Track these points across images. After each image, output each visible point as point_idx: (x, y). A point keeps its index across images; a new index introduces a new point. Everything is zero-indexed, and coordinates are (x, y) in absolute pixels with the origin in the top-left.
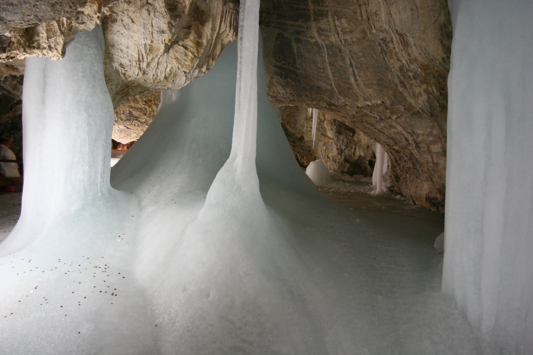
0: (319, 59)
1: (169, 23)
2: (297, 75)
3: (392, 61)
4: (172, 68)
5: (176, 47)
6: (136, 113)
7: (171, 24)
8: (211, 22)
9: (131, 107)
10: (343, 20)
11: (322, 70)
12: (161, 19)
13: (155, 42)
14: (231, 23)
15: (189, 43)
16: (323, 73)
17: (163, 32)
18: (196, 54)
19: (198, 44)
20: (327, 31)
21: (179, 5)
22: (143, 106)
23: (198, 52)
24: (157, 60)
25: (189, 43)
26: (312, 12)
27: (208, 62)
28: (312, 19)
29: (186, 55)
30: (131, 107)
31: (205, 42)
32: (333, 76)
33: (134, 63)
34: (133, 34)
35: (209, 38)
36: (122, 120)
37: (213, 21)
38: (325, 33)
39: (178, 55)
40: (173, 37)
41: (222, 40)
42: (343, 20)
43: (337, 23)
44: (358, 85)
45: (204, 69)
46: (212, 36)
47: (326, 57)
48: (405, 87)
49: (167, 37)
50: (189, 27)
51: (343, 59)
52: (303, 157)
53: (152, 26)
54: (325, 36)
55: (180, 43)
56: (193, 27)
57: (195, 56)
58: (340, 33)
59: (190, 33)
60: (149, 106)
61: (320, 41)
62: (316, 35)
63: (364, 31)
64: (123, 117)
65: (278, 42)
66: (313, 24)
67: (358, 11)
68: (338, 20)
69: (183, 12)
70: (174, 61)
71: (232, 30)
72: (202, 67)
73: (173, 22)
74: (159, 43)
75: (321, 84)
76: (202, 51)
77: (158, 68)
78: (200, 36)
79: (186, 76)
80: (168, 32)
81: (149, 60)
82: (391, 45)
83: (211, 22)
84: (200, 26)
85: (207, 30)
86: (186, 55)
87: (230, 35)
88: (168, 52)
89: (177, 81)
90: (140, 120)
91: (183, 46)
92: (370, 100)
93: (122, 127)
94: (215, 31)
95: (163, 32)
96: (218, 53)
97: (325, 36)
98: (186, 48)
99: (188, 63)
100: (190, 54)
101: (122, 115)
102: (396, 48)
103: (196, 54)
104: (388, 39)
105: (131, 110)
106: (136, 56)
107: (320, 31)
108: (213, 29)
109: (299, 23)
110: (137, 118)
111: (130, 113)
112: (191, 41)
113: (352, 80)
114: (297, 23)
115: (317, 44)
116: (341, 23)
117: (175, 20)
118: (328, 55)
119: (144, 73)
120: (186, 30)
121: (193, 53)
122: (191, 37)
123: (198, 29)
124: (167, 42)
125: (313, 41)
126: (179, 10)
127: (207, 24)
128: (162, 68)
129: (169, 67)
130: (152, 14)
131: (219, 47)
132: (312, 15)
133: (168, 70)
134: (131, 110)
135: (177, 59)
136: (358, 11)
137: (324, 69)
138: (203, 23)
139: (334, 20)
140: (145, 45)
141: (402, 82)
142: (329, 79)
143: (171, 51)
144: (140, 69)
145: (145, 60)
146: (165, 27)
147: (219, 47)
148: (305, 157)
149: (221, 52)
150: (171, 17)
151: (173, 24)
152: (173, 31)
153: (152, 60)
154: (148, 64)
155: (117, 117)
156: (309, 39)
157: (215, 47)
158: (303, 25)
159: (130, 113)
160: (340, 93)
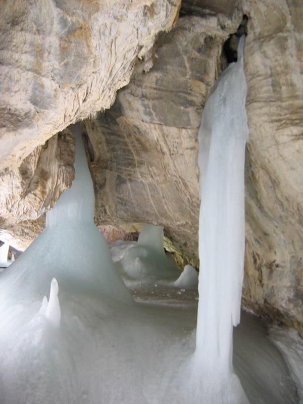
0: (144, 192)
1: (22, 183)
2: (133, 204)
3: (183, 196)
4: (27, 207)
5: (30, 195)
6: (27, 231)
7: (23, 183)
8: (51, 179)
9: (23, 226)
10: (154, 168)
11: (147, 200)
12: (17, 179)
13: (14, 193)
14: (63, 179)
15: (38, 192)
16: (148, 202)
17: (18, 188)
18: (42, 199)
19: (43, 193)
20: (145, 174)
21: (29, 171)
22: (31, 226)
23: (43, 197)
24: (17, 203)
25: (38, 192)
26: (136, 161)
27: (51, 203)
28: (137, 165)
29: (36, 199)
30: (23, 226)
31: (47, 190)
32: (155, 204)
33: (4, 205)
34: (3, 188)
35: (51, 188)
36: (17, 235)
37: (52, 178)
38: (144, 175)
39: (31, 200)
40: (24, 190)
41: (60, 189)
42: (154, 168)
43: (151, 169)
44: (170, 211)
45: (49, 207)
46: (52, 187)
47: (149, 191)
48: (195, 213)
49: (20, 190)
50: (37, 182)
51: (158, 193)
52: (190, 260)
53: (12, 184)
54: (145, 177)
55: (32, 192)
56: (40, 182)
57: (41, 200)
58: (154, 176)
59: (38, 186)
60: (35, 226)
61: (143, 181)
62: (140, 177)
63: (165, 176)
64: (18, 233)
65: (118, 181)
66: (137, 169)
67: (160, 162)
68: (151, 167)
69: (31, 175)
70: (28, 203)
71: (64, 184)
72: (48, 206)
73: (24, 181)
74: (18, 192)
75: (148, 210)
76: (46, 197)
77: (19, 207)
78: (44, 187)
79: (37, 212)
80: (21, 187)
81: (13, 204)
82: (180, 185)
83: (51, 179)
84: (44, 181)
85: (49, 184)
86: (36, 199)
87: (64, 186)
88: (24, 198)
89: (32, 215)
90: (31, 235)
91: (34, 194)
92: (179, 221)
93: (19, 240)
94: (54, 183)
95: (18, 188)
96: (58, 197)
97: (145, 177)
98: (35, 195)
99: (37, 204)
100: (38, 199)
101: (17, 232)
102: (107, 211)
103: (42, 199)
104: (178, 182)
105: (23, 228)
106: (5, 201)
107: (142, 174)
108: (53, 183)
109: (130, 168)
110: (27, 234)
111: (23, 231)
112: (39, 191)
113: (166, 207)
114: (128, 169)
115: (142, 182)
116: (153, 170)
117: (25, 180)
118: (150, 190)
119: (10, 211)
120: (36, 184)
121: (40, 198)
122: (39, 189)
123: (43, 183)
124: (20, 193)
125: (139, 180)
126: (29, 174)
127: (49, 180)
128: (21, 207)
129: (26, 207)
130: (12, 177)
131: (58, 193)
132: (136, 163)
133: (25, 209)
134: (23, 228)
135: (30, 202)
136: (160, 162)
137: (148, 199)
138: (46, 179)
139: (148, 167)
140: (9, 195)
141: (192, 210)
142: (152, 206)
143: (26, 197)
144: (7, 208)
145: (10, 203)
146: (19, 185)
147: (58, 193)
148: (192, 260)
149: (59, 196)
150: (23, 179)
151: (24, 182)
152: (24, 187)
153: (15, 203)
154: (13, 206)
155: (14, 233)
156: (137, 179)
157: (55, 193)
158: (132, 170)
159: (23, 231)
160: (161, 216)
